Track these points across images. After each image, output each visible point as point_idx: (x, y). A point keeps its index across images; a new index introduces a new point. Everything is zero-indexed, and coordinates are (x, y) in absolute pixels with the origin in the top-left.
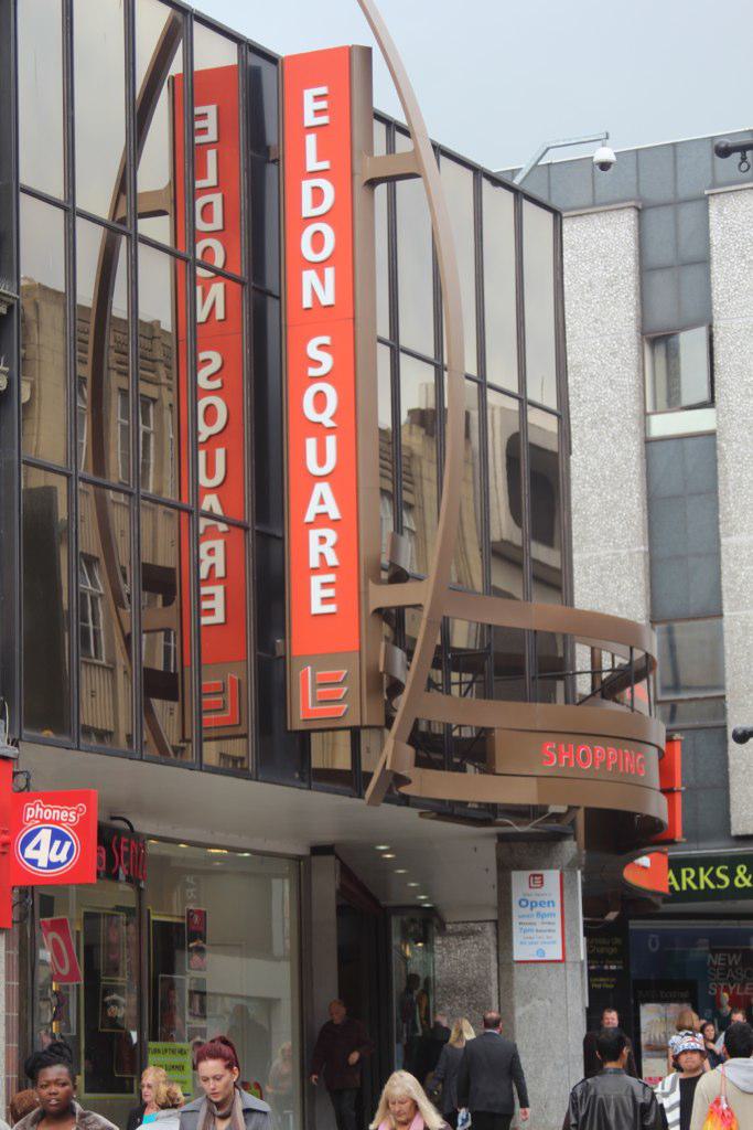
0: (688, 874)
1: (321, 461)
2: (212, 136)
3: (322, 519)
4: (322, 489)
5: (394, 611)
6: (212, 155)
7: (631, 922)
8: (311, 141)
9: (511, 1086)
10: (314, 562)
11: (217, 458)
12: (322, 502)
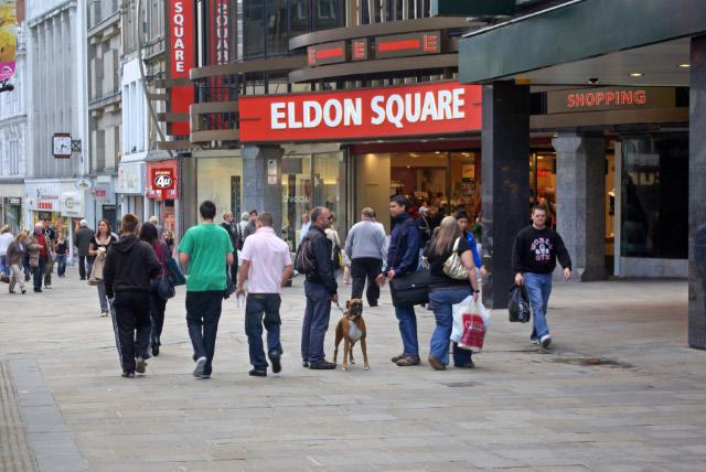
1: (179, 33)
3: (179, 48)
4: (179, 41)
5: (214, 116)
7: (532, 118)
9: (229, 60)
10: (177, 58)
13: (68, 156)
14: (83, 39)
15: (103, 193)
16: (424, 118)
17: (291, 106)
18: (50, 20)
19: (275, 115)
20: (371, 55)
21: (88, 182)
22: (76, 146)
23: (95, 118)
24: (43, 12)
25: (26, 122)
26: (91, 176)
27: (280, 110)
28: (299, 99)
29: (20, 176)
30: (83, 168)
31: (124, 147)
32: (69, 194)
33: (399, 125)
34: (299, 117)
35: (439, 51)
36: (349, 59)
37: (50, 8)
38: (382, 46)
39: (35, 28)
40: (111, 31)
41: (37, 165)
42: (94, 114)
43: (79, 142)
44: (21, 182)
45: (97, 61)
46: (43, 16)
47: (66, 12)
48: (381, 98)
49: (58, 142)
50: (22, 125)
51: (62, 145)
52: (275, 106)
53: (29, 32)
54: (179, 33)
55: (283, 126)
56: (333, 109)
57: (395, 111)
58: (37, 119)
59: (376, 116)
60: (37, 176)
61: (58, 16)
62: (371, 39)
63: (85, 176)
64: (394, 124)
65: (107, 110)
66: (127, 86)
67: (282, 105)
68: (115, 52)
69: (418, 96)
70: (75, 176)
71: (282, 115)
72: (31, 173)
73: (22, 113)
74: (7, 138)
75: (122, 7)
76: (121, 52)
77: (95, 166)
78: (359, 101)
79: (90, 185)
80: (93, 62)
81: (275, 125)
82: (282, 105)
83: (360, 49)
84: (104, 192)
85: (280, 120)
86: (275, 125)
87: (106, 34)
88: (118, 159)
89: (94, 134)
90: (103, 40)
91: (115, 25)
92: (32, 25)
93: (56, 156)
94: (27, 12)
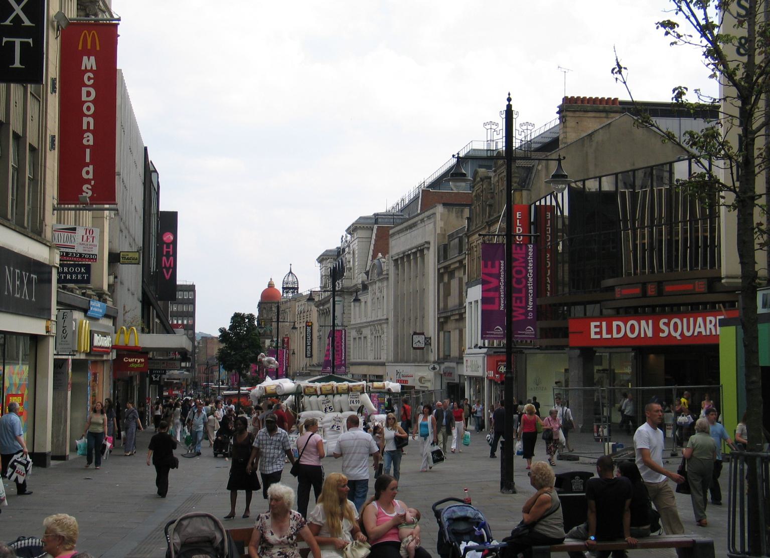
0: (711, 322)
1: (88, 123)
2: (549, 217)
6: (549, 221)
8: (518, 220)
11: (26, 18)
12: (700, 327)
13: (422, 348)
14: (435, 269)
15: (450, 374)
16: (696, 334)
17: (604, 324)
18: (409, 256)
19: (593, 330)
20: (660, 293)
21: (437, 366)
22: (428, 341)
23: (442, 324)
24: (403, 249)
25: (387, 323)
26: (439, 362)
27: (596, 327)
28: (609, 320)
29: (382, 360)
30: (433, 357)
31: (467, 344)
32: (421, 374)
33: (679, 338)
34: (609, 331)
35: (706, 291)
36: (644, 294)
37: (408, 247)
38: (668, 288)
39: (396, 261)
40: (457, 265)
41: (396, 354)
42: (442, 320)
43: (430, 338)
44: (383, 364)
45: (445, 284)
46: (404, 253)
47: (422, 251)
48: (666, 320)
49: (416, 338)
50: (385, 326)
51: (419, 341)
52: (593, 324)
53: (392, 264)
54: (88, 123)
55: (598, 337)
56: (632, 326)
57: (676, 330)
58: (396, 321)
59: (663, 331)
60: (397, 360)
61: (415, 253)
62: (660, 284)
63: (434, 362)
64: (676, 337)
65: (452, 318)
66: (471, 303)
67: (598, 323)
68: (461, 280)
69: (692, 320)
70: (427, 362)
71: (598, 330)
72: (391, 358)
73: (385, 317)
74: (372, 334)
75: (468, 250)
76: (465, 279)
77: (441, 355)
78: (650, 322)
79: (438, 368)
80: (441, 285)
81: (593, 336)
82: (598, 323)
83: (651, 289)
84: (451, 373)
85: (596, 333)
86: (593, 336)
87: (452, 267)
88: (461, 352)
89: (442, 334)
90: (449, 270)
91: (461, 262)
92: (394, 258)
93: (415, 348)
94: (390, 249)
